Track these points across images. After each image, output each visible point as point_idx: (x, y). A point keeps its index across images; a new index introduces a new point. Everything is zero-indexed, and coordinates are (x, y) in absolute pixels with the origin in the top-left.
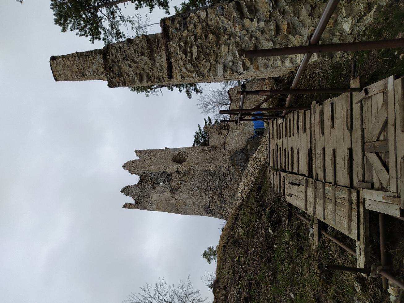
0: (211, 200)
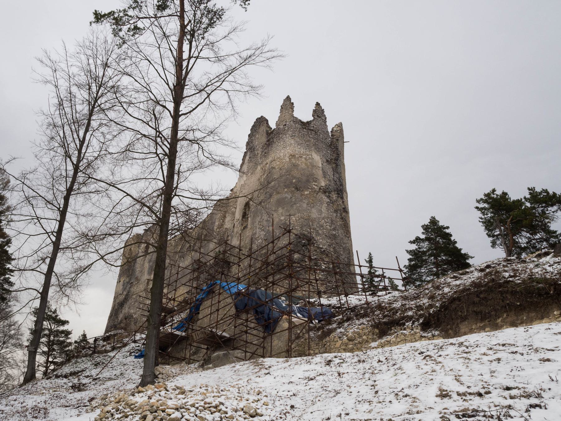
0: (324, 251)
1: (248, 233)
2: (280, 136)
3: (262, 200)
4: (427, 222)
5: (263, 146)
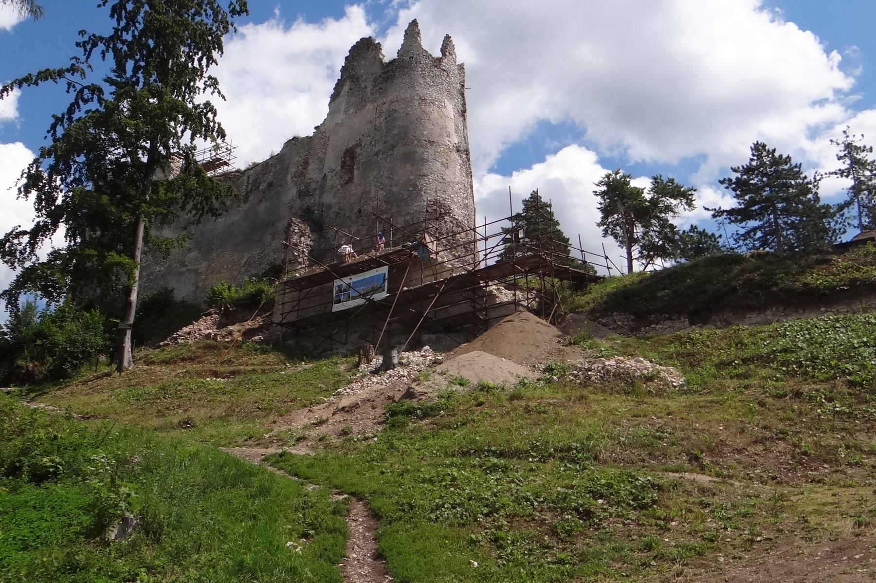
1: (355, 190)
2: (406, 70)
3: (379, 151)
4: (527, 196)
5: (375, 80)
